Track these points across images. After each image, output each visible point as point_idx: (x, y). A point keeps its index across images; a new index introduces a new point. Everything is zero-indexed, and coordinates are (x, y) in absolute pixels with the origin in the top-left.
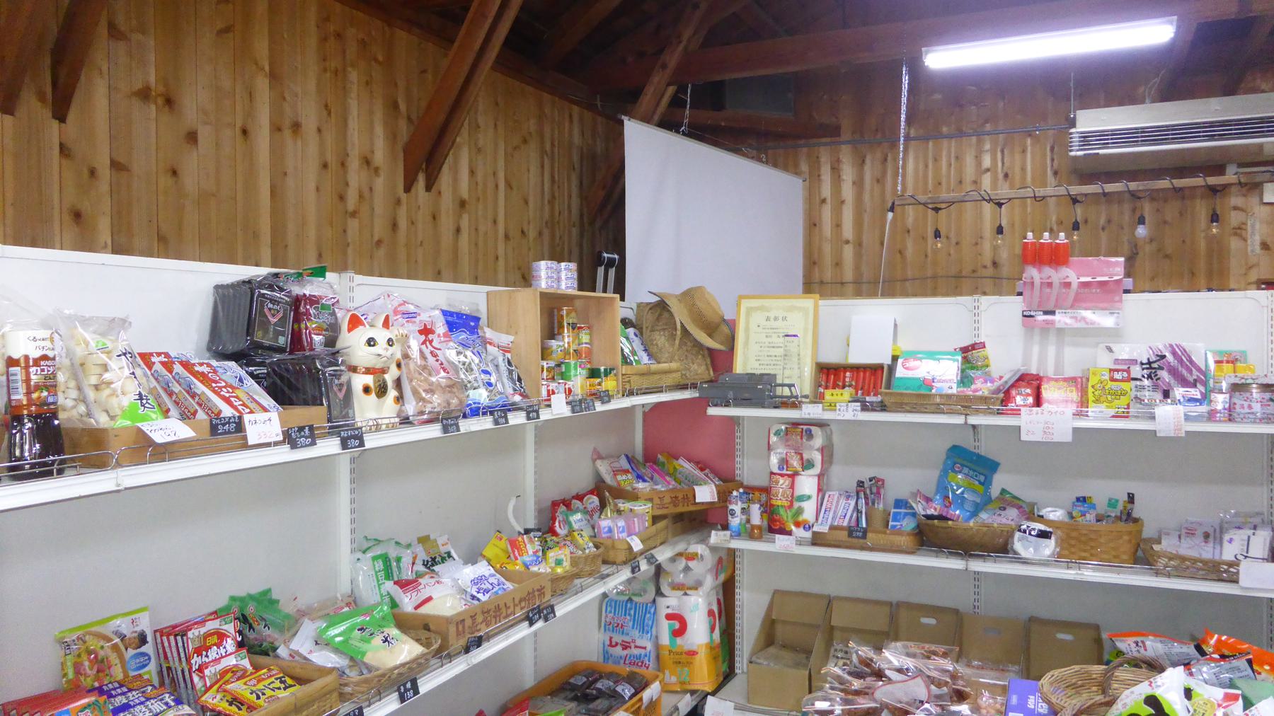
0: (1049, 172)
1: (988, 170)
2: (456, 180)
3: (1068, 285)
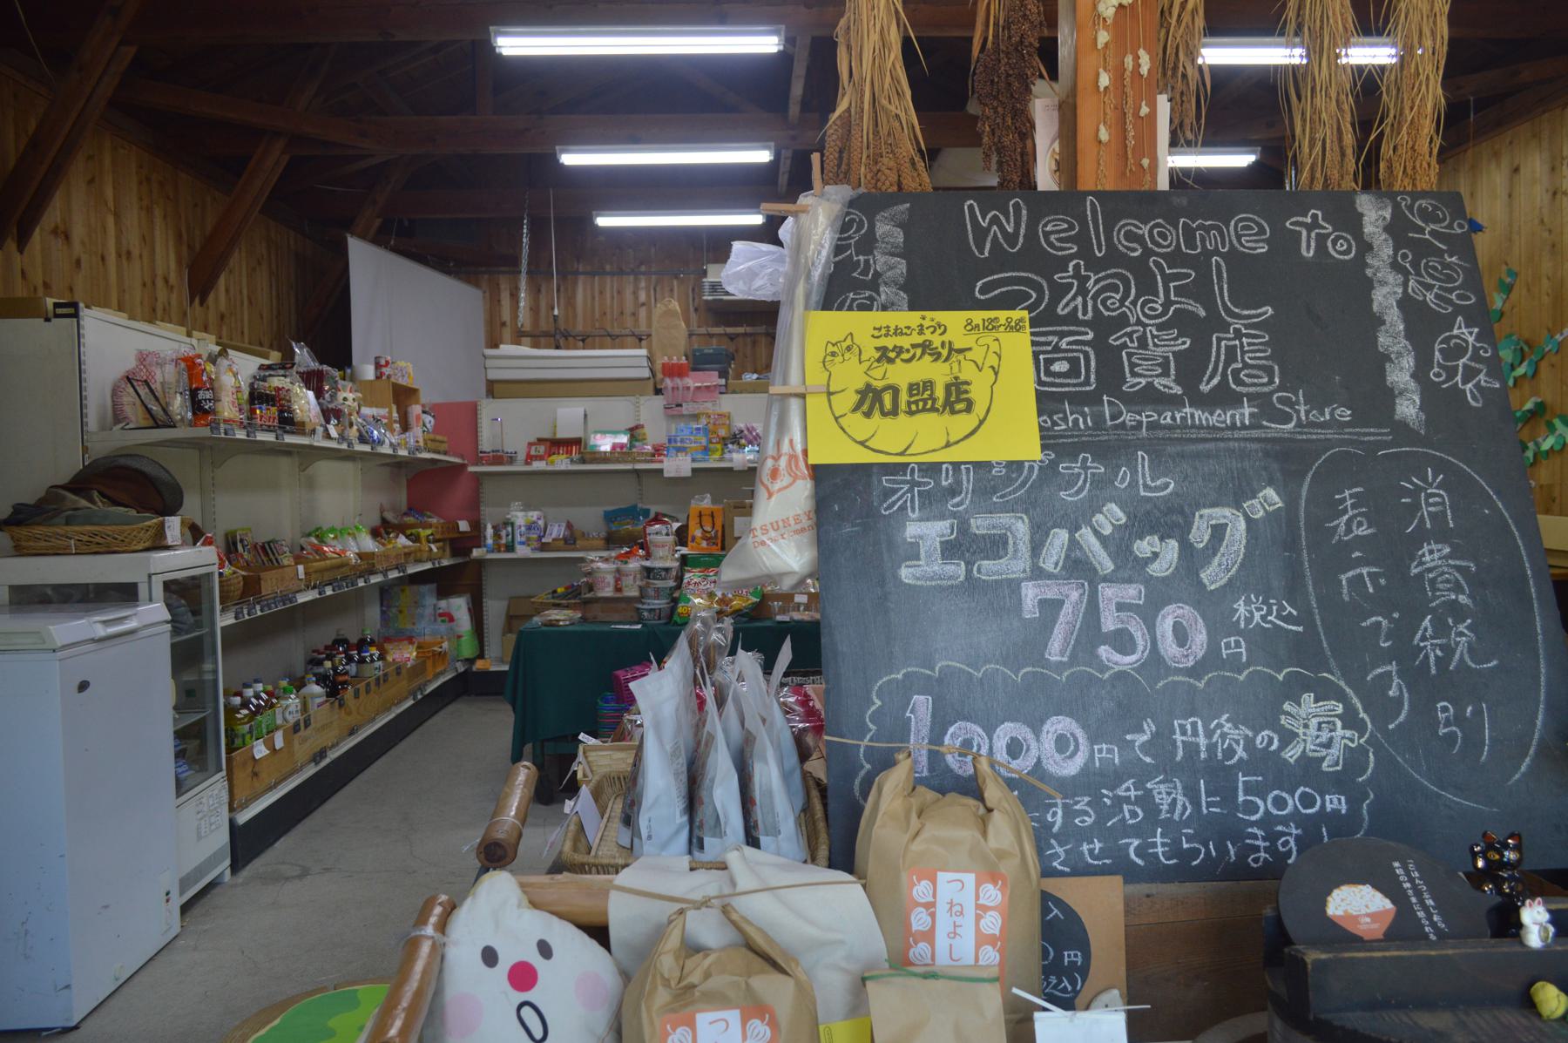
0: (692, 309)
1: (643, 304)
2: (217, 299)
3: (688, 388)
